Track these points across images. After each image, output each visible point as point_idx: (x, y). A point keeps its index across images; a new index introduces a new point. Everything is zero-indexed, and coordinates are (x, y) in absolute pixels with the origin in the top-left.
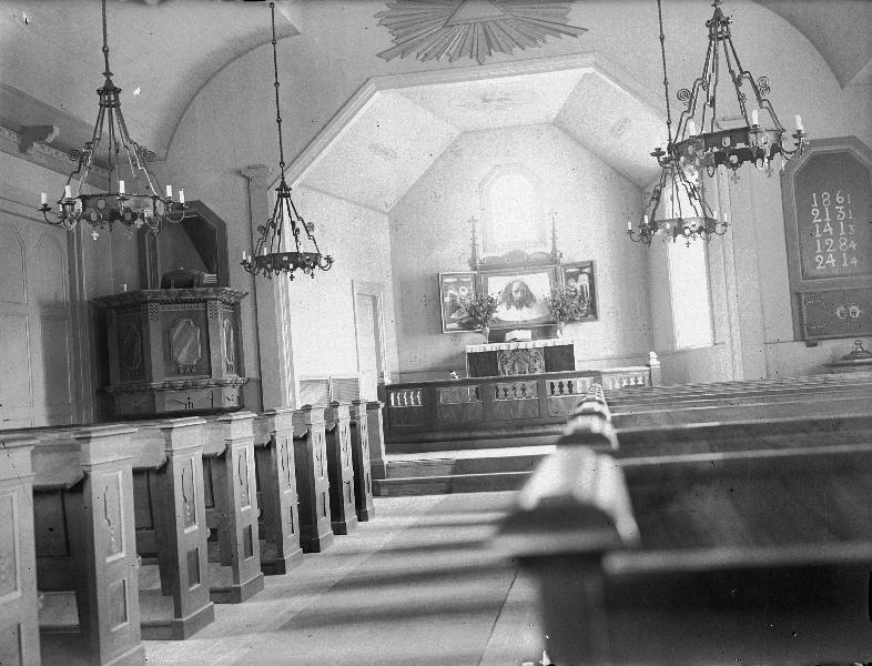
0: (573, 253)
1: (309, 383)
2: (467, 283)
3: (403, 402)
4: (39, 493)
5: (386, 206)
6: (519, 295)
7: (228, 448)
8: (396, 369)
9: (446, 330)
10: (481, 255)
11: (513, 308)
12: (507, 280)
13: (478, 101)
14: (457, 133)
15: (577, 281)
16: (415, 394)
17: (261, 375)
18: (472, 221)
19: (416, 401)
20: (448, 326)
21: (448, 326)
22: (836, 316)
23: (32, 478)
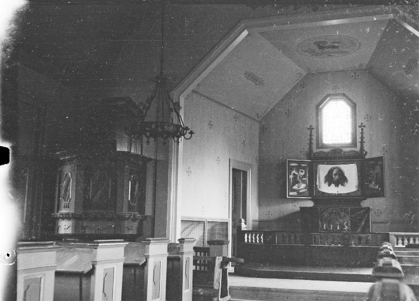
0: (373, 152)
1: (189, 223)
2: (304, 168)
3: (256, 240)
4: (126, 266)
5: (258, 117)
6: (337, 177)
7: (94, 268)
8: (257, 218)
9: (289, 196)
10: (315, 150)
11: (333, 185)
12: (330, 167)
13: (316, 48)
14: (304, 73)
15: (374, 170)
16: (252, 236)
17: (154, 214)
18: (311, 129)
19: (260, 240)
20: (291, 194)
21: (291, 194)
22: (357, 250)
23: (123, 260)
